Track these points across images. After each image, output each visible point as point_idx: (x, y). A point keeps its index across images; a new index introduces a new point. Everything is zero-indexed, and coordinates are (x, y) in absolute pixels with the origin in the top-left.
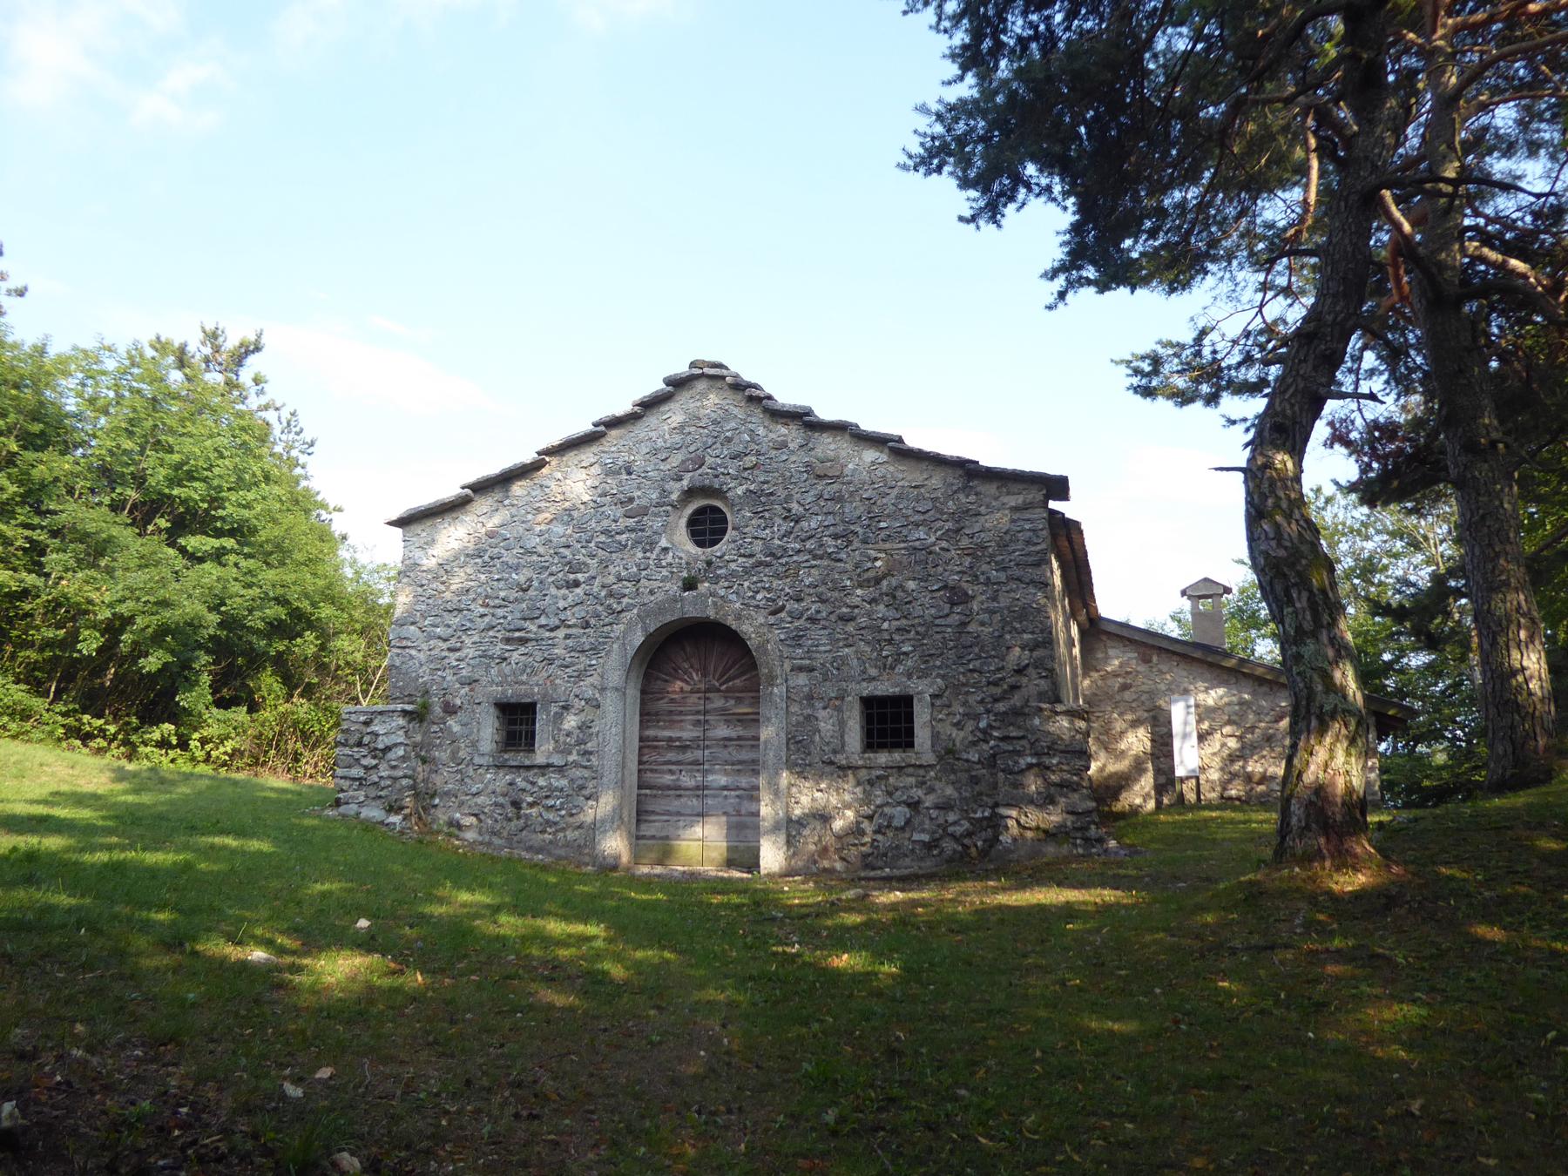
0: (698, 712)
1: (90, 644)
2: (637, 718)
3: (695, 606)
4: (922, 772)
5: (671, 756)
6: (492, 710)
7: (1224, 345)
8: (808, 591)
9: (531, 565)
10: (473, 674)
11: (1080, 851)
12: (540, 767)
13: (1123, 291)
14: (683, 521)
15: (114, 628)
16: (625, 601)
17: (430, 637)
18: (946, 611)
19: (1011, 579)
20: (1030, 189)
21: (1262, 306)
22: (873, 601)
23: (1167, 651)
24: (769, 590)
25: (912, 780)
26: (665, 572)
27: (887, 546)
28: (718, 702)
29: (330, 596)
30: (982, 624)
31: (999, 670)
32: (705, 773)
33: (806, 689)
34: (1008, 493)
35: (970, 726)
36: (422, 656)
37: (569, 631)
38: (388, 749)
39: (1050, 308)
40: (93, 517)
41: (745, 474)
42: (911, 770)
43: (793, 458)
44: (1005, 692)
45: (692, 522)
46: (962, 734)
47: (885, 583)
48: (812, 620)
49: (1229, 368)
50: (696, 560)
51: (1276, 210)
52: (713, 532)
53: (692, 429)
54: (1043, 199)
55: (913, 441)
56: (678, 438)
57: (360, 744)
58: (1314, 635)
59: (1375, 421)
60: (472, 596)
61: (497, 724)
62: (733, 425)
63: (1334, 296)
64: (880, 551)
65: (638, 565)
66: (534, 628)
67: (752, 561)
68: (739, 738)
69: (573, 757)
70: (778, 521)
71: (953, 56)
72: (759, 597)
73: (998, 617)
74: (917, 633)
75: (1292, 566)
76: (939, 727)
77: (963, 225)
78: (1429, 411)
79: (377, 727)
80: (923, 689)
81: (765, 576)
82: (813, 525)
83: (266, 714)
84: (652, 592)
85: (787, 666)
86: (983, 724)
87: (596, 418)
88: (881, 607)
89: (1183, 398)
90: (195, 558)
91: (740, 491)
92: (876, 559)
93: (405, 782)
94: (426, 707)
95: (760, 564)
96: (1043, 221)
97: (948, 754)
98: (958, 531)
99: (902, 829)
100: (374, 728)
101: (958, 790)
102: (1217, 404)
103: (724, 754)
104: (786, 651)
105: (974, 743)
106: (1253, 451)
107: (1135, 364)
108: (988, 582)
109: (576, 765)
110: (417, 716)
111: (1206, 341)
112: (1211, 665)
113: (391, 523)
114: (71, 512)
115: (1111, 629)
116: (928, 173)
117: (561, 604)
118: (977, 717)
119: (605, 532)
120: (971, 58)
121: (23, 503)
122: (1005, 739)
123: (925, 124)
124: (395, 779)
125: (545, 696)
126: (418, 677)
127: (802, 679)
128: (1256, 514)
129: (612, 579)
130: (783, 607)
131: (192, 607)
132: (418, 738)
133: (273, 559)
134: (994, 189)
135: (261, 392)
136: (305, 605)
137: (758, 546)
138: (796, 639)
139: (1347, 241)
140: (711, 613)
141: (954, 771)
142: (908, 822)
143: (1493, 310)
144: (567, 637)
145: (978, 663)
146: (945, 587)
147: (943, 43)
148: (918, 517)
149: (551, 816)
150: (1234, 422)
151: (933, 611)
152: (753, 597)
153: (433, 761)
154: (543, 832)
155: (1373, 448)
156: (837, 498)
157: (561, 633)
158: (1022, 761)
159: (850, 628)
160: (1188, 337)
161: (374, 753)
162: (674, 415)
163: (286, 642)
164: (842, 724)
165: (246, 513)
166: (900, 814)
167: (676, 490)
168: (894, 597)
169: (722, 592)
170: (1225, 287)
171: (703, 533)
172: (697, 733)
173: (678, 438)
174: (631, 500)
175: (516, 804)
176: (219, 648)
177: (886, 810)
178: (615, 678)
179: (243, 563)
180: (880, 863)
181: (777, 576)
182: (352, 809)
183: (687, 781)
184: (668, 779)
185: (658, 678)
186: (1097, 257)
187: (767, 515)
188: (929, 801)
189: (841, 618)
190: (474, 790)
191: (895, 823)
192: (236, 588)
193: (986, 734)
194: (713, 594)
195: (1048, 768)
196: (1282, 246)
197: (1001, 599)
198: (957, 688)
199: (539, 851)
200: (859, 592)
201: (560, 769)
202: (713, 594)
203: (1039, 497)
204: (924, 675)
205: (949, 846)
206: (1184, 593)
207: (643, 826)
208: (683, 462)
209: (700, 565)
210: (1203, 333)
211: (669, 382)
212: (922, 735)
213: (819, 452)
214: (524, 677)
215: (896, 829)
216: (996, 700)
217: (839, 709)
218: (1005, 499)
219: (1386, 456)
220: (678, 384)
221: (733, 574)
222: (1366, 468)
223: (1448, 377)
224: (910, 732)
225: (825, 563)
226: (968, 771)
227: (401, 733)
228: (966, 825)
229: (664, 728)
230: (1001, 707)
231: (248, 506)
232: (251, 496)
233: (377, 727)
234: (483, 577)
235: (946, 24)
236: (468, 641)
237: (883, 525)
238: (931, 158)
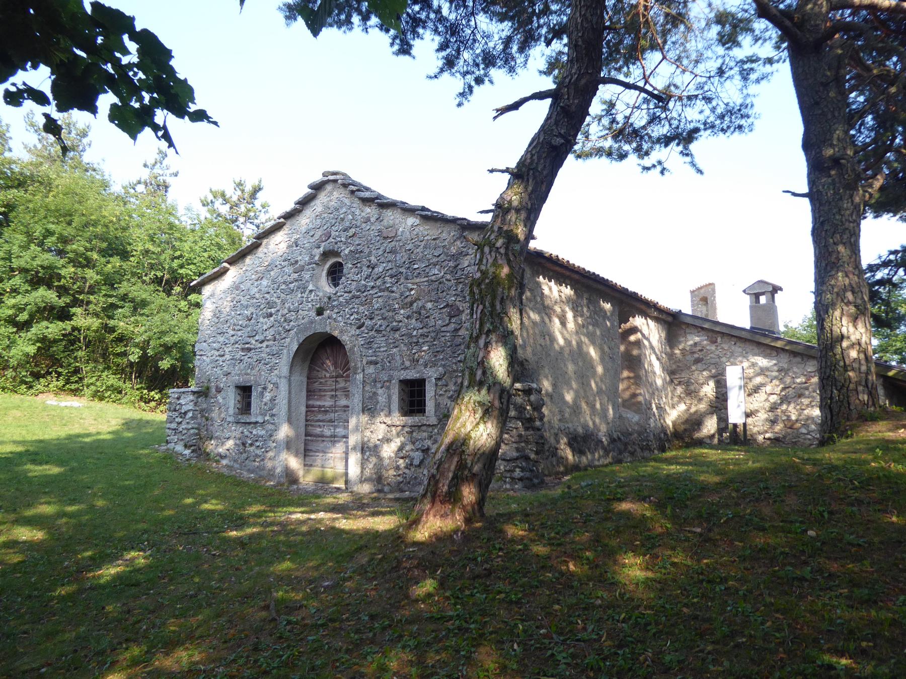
0: (332, 390)
2: (304, 393)
4: (430, 429)
5: (320, 417)
8: (378, 312)
11: (508, 486)
14: (324, 273)
15: (144, 346)
16: (292, 323)
22: (408, 317)
23: (729, 335)
24: (357, 313)
25: (425, 434)
27: (418, 280)
32: (335, 427)
33: (373, 376)
38: (185, 413)
40: (139, 291)
47: (415, 304)
53: (326, 215)
62: (344, 210)
66: (254, 342)
67: (350, 295)
70: (365, 268)
76: (440, 400)
80: (431, 374)
84: (303, 318)
85: (364, 362)
91: (347, 252)
92: (412, 289)
94: (208, 388)
95: (354, 297)
100: (181, 401)
112: (759, 344)
115: (689, 320)
117: (265, 327)
119: (284, 283)
121: (105, 284)
127: (371, 370)
129: (286, 311)
130: (364, 323)
139: (578, 14)
142: (422, 462)
146: (447, 306)
151: (440, 322)
154: (254, 461)
159: (397, 335)
162: (318, 205)
164: (389, 397)
166: (417, 456)
167: (317, 253)
174: (297, 262)
175: (244, 444)
180: (406, 488)
183: (327, 432)
200: (402, 312)
204: (434, 365)
207: (307, 459)
209: (326, 300)
212: (430, 405)
213: (385, 223)
217: (388, 388)
220: (317, 188)
225: (386, 293)
227: (192, 404)
229: (317, 400)
233: (182, 401)
236: (227, 350)
237: (416, 266)
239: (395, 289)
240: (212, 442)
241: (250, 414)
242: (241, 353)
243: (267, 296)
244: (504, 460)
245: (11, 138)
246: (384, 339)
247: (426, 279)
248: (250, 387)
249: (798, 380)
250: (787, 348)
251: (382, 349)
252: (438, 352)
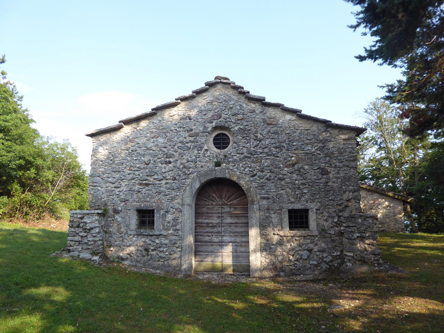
0: (219, 213)
3: (219, 173)
4: (313, 238)
5: (209, 230)
6: (135, 212)
8: (266, 168)
9: (150, 154)
10: (125, 195)
11: (377, 268)
12: (156, 235)
14: (212, 139)
16: (191, 170)
17: (107, 182)
18: (320, 177)
19: (344, 166)
24: (250, 167)
25: (309, 241)
26: (207, 159)
27: (296, 152)
28: (227, 209)
29: (40, 155)
30: (334, 182)
31: (341, 200)
32: (222, 236)
33: (266, 206)
34: (342, 134)
35: (330, 220)
36: (103, 189)
37: (167, 181)
38: (92, 229)
41: (239, 122)
42: (309, 237)
43: (258, 117)
44: (343, 208)
46: (327, 223)
47: (296, 166)
48: (268, 179)
52: (223, 144)
53: (216, 103)
57: (78, 227)
61: (137, 218)
62: (233, 102)
64: (294, 154)
65: (196, 156)
66: (152, 180)
67: (242, 156)
68: (236, 223)
72: (247, 170)
73: (340, 180)
74: (309, 185)
79: (86, 220)
80: (313, 206)
82: (267, 143)
83: (16, 199)
85: (259, 197)
87: (177, 97)
88: (295, 175)
91: (236, 128)
92: (292, 157)
95: (246, 157)
97: (323, 231)
98: (323, 147)
101: (327, 245)
103: (230, 229)
104: (258, 191)
105: (332, 227)
108: (336, 167)
109: (172, 234)
110: (103, 215)
113: (88, 135)
117: (164, 170)
118: (333, 217)
124: (95, 241)
125: (158, 207)
126: (102, 198)
127: (265, 202)
129: (185, 161)
130: (256, 174)
133: (18, 142)
135: (5, 78)
136: (31, 159)
137: (245, 150)
138: (262, 187)
140: (227, 176)
141: (325, 238)
142: (308, 257)
144: (166, 183)
148: (307, 141)
149: (162, 255)
151: (315, 177)
152: (244, 170)
153: (110, 232)
154: (159, 261)
156: (276, 133)
157: (164, 182)
158: (355, 235)
159: (283, 183)
161: (85, 230)
163: (22, 172)
165: (7, 124)
166: (305, 254)
167: (210, 127)
168: (300, 171)
169: (231, 168)
171: (219, 144)
172: (218, 221)
174: (192, 130)
175: (147, 250)
177: (300, 252)
179: (6, 143)
180: (298, 273)
181: (253, 162)
182: (76, 254)
183: (215, 239)
184: (207, 238)
185: (202, 199)
187: (248, 138)
189: (280, 179)
190: (128, 244)
191: (303, 257)
194: (228, 169)
195: (364, 238)
197: (341, 174)
198: (325, 206)
199: (157, 268)
200: (286, 169)
201: (165, 236)
204: (313, 201)
205: (324, 266)
208: (213, 116)
209: (222, 157)
211: (207, 84)
212: (312, 224)
213: (268, 114)
214: (148, 199)
215: (304, 259)
220: (210, 85)
221: (235, 160)
224: (290, 218)
227: (97, 222)
228: (330, 258)
229: (205, 219)
231: (6, 121)
232: (9, 117)
233: (86, 220)
234: (129, 158)
236: (123, 184)
237: (294, 144)
239: (279, 155)
240: (112, 249)
241: (153, 228)
243: (165, 149)
244: (374, 254)
246: (274, 184)
247: (302, 152)
248: (152, 212)
249: (370, 202)
250: (368, 188)
251: (272, 190)
252: (315, 194)
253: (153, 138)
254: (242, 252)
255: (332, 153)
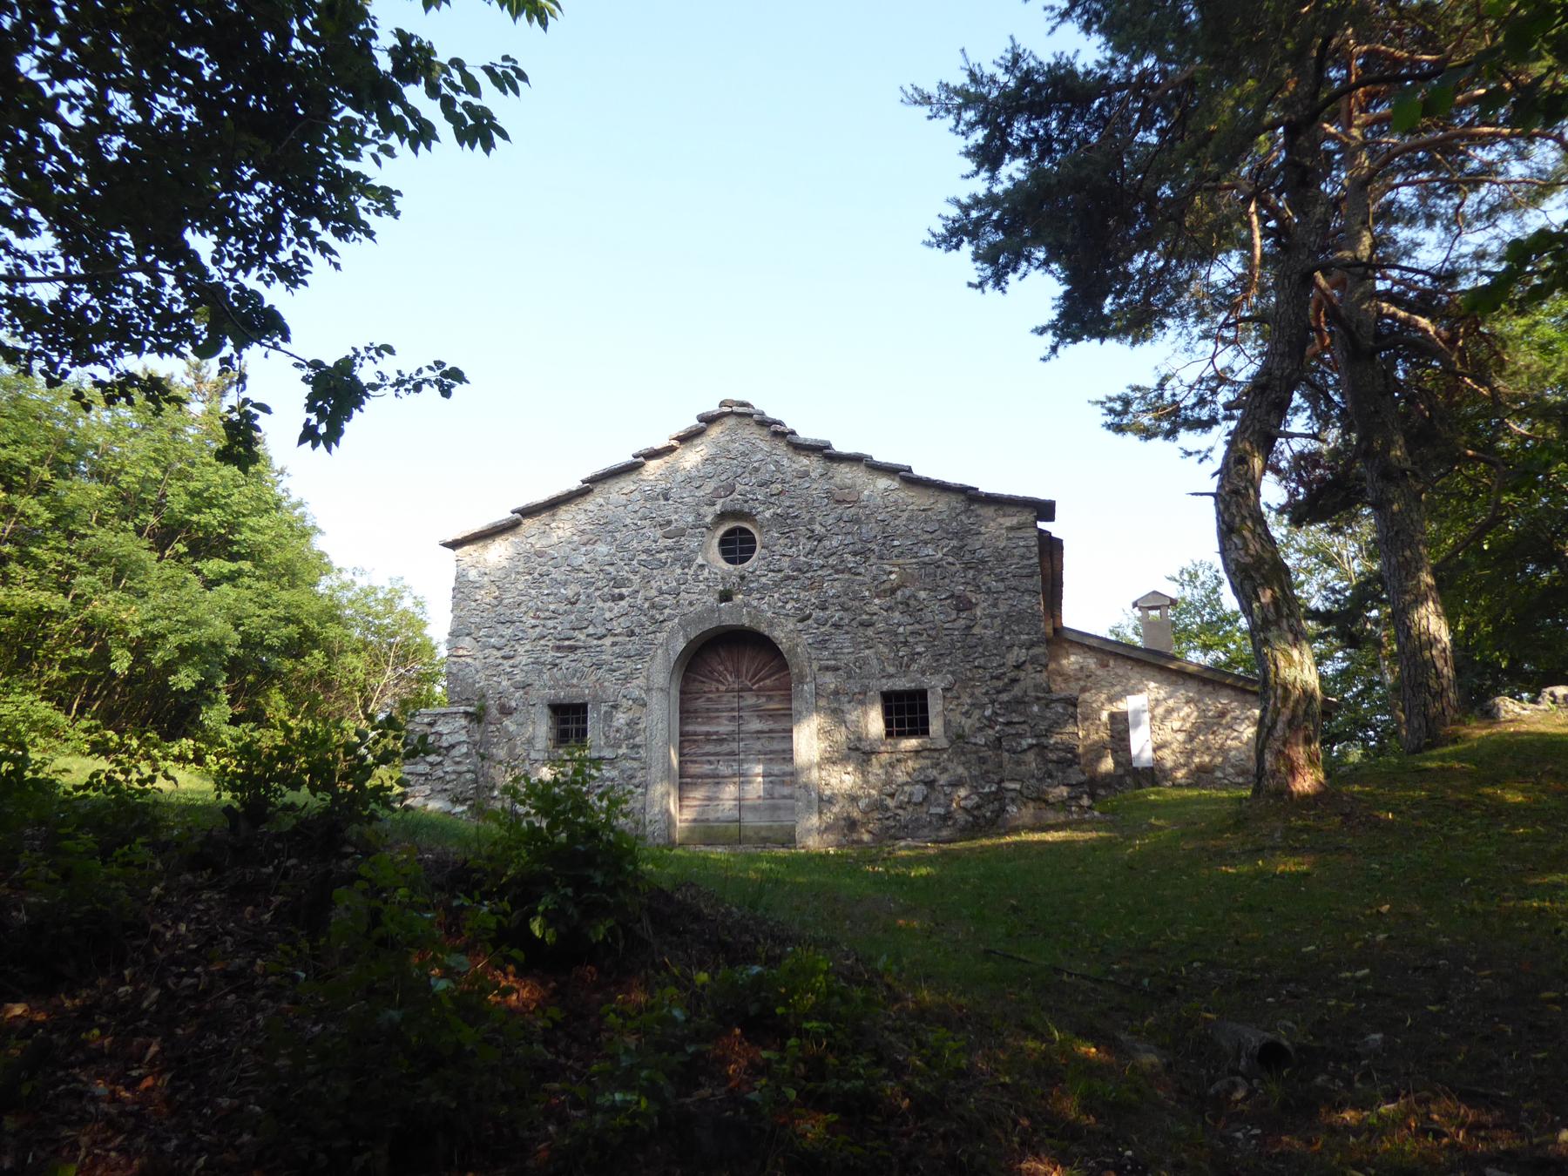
0: (733, 710)
1: (121, 663)
3: (729, 615)
4: (936, 755)
5: (709, 748)
7: (1181, 391)
9: (579, 580)
13: (1096, 341)
14: (716, 541)
15: (140, 650)
16: (667, 611)
17: (485, 647)
20: (1030, 264)
21: (1214, 356)
23: (1123, 656)
24: (797, 600)
26: (702, 586)
27: (901, 561)
29: (331, 615)
30: (985, 627)
32: (740, 762)
38: (452, 746)
39: (1044, 359)
40: (126, 543)
45: (722, 542)
47: (899, 593)
48: (836, 626)
49: (1186, 408)
50: (730, 575)
51: (1224, 271)
52: (742, 551)
54: (1041, 271)
55: (919, 471)
56: (710, 468)
58: (1277, 624)
59: (1301, 453)
60: (523, 609)
62: (759, 456)
63: (1281, 355)
65: (677, 581)
66: (582, 637)
67: (780, 575)
68: (771, 731)
69: (623, 751)
71: (968, 154)
72: (788, 606)
73: (998, 621)
75: (1258, 570)
77: (972, 290)
78: (1347, 443)
80: (935, 684)
81: (792, 589)
82: (835, 543)
84: (691, 604)
85: (815, 666)
86: (988, 713)
87: (636, 451)
88: (897, 614)
89: (1148, 434)
90: (210, 584)
91: (768, 514)
93: (469, 776)
95: (788, 578)
96: (1039, 290)
97: (958, 739)
98: (961, 548)
99: (921, 804)
102: (1175, 439)
103: (758, 746)
104: (814, 654)
105: (981, 729)
106: (1221, 479)
107: (1109, 405)
109: (625, 757)
110: (477, 717)
111: (1168, 386)
113: (446, 545)
114: (102, 537)
116: (948, 250)
117: (608, 615)
118: (983, 707)
120: (988, 157)
122: (1009, 724)
123: (954, 212)
124: (460, 773)
125: (595, 697)
126: (475, 682)
128: (1227, 531)
129: (654, 593)
131: (219, 627)
132: (477, 737)
134: (999, 264)
136: (313, 625)
137: (786, 562)
138: (822, 643)
140: (746, 622)
141: (964, 754)
142: (926, 798)
143: (1399, 356)
144: (614, 644)
145: (982, 661)
146: (952, 596)
147: (961, 143)
150: (1190, 454)
155: (1299, 475)
156: (855, 520)
157: (608, 641)
159: (870, 632)
160: (1152, 383)
165: (259, 538)
167: (709, 514)
169: (755, 603)
170: (1182, 342)
173: (710, 468)
174: (669, 523)
176: (235, 667)
178: (660, 678)
181: (804, 588)
184: (706, 768)
186: (1077, 320)
188: (943, 779)
192: (252, 608)
193: (991, 722)
196: (1225, 300)
198: (965, 683)
200: (877, 601)
202: (747, 605)
203: (1031, 518)
204: (936, 671)
206: (1135, 605)
209: (735, 579)
210: (1166, 379)
211: (702, 418)
212: (936, 726)
213: (837, 480)
214: (575, 681)
216: (999, 692)
218: (1001, 520)
219: (1311, 482)
220: (709, 420)
222: (1293, 494)
223: (1365, 412)
224: (925, 722)
225: (846, 576)
226: (976, 752)
228: (976, 799)
229: (703, 724)
230: (1005, 697)
232: (264, 522)
235: (962, 127)
236: (521, 650)
238: (953, 236)
242: (551, 653)
243: (611, 569)
245: (305, 283)
253: (584, 545)
254: (784, 797)
255: (983, 561)
